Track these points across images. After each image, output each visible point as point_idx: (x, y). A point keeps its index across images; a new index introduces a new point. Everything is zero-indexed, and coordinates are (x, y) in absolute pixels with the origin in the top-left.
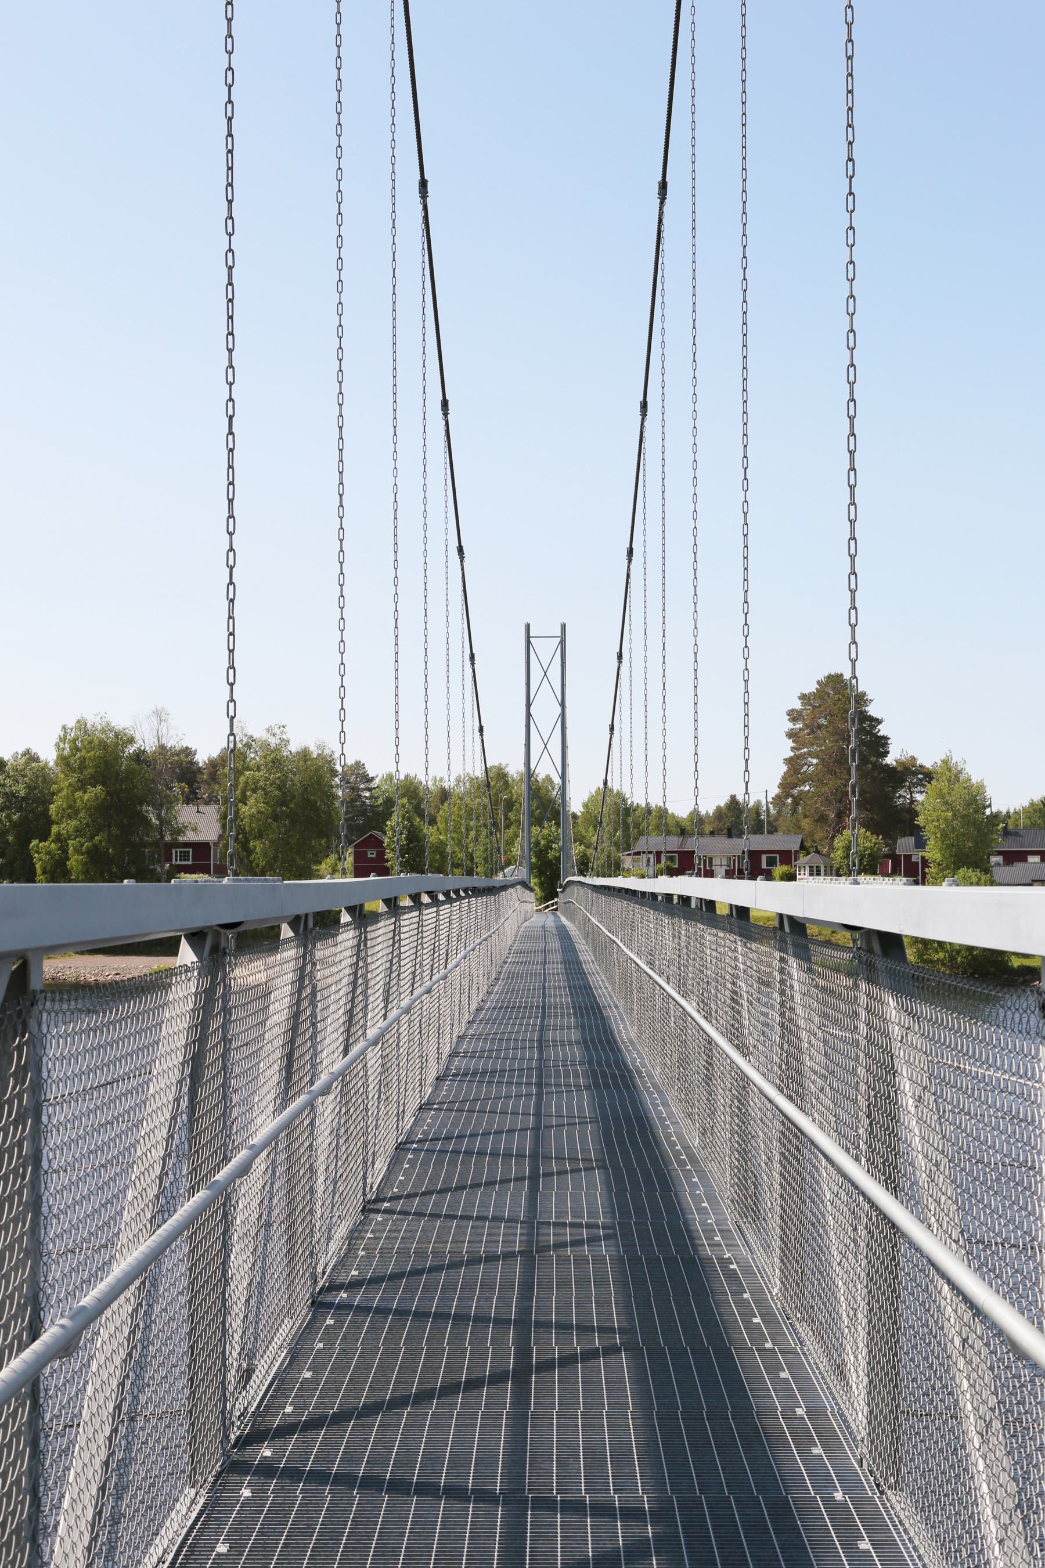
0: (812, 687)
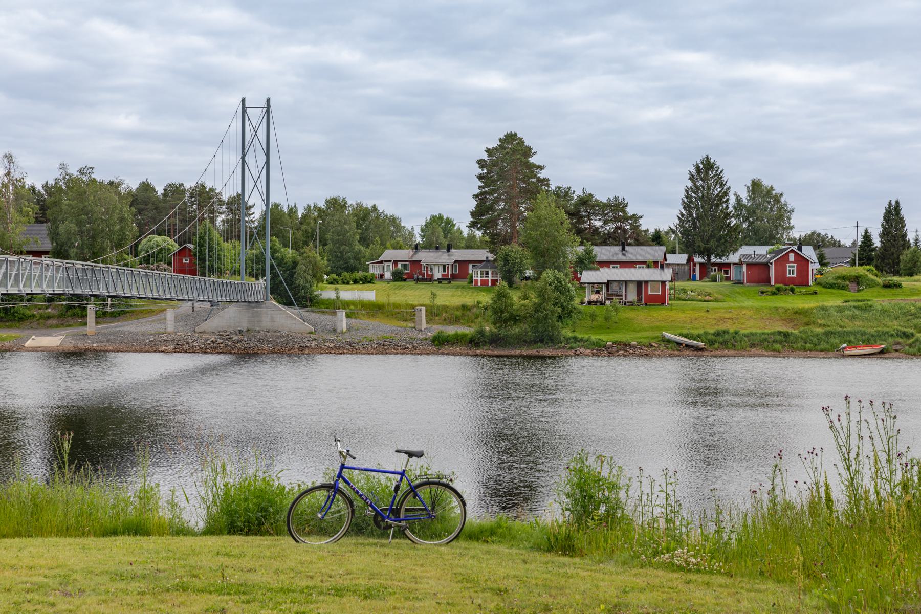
0: (494, 144)
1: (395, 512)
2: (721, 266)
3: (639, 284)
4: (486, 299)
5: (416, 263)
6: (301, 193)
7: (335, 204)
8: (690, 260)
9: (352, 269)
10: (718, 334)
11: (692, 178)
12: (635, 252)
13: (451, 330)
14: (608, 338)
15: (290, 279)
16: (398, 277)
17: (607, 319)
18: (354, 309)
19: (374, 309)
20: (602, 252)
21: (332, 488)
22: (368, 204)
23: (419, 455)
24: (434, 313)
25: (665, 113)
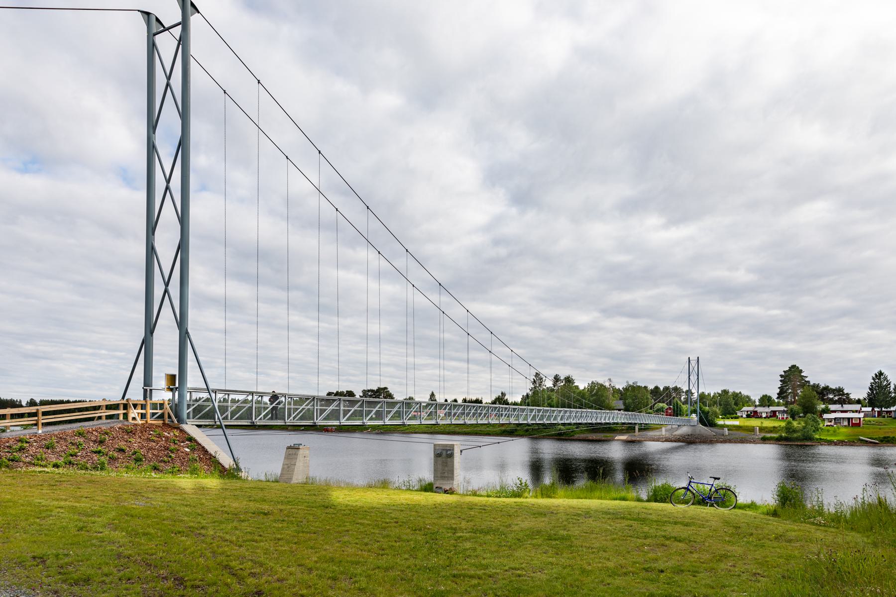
0: (787, 369)
1: (710, 498)
2: (887, 412)
3: (849, 419)
4: (783, 424)
5: (756, 412)
6: (712, 389)
7: (725, 392)
8: (873, 410)
9: (730, 414)
10: (885, 438)
11: (873, 379)
12: (847, 407)
13: (768, 435)
14: (835, 439)
15: (707, 418)
16: (748, 416)
17: (834, 432)
18: (730, 428)
19: (738, 428)
20: (832, 407)
21: (687, 489)
22: (738, 391)
23: (719, 479)
24: (762, 429)
25: (865, 354)
